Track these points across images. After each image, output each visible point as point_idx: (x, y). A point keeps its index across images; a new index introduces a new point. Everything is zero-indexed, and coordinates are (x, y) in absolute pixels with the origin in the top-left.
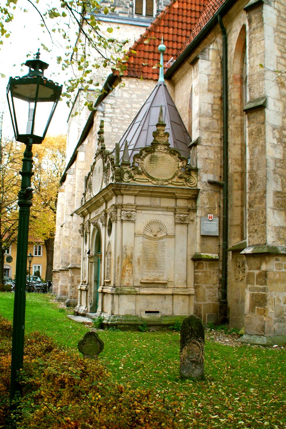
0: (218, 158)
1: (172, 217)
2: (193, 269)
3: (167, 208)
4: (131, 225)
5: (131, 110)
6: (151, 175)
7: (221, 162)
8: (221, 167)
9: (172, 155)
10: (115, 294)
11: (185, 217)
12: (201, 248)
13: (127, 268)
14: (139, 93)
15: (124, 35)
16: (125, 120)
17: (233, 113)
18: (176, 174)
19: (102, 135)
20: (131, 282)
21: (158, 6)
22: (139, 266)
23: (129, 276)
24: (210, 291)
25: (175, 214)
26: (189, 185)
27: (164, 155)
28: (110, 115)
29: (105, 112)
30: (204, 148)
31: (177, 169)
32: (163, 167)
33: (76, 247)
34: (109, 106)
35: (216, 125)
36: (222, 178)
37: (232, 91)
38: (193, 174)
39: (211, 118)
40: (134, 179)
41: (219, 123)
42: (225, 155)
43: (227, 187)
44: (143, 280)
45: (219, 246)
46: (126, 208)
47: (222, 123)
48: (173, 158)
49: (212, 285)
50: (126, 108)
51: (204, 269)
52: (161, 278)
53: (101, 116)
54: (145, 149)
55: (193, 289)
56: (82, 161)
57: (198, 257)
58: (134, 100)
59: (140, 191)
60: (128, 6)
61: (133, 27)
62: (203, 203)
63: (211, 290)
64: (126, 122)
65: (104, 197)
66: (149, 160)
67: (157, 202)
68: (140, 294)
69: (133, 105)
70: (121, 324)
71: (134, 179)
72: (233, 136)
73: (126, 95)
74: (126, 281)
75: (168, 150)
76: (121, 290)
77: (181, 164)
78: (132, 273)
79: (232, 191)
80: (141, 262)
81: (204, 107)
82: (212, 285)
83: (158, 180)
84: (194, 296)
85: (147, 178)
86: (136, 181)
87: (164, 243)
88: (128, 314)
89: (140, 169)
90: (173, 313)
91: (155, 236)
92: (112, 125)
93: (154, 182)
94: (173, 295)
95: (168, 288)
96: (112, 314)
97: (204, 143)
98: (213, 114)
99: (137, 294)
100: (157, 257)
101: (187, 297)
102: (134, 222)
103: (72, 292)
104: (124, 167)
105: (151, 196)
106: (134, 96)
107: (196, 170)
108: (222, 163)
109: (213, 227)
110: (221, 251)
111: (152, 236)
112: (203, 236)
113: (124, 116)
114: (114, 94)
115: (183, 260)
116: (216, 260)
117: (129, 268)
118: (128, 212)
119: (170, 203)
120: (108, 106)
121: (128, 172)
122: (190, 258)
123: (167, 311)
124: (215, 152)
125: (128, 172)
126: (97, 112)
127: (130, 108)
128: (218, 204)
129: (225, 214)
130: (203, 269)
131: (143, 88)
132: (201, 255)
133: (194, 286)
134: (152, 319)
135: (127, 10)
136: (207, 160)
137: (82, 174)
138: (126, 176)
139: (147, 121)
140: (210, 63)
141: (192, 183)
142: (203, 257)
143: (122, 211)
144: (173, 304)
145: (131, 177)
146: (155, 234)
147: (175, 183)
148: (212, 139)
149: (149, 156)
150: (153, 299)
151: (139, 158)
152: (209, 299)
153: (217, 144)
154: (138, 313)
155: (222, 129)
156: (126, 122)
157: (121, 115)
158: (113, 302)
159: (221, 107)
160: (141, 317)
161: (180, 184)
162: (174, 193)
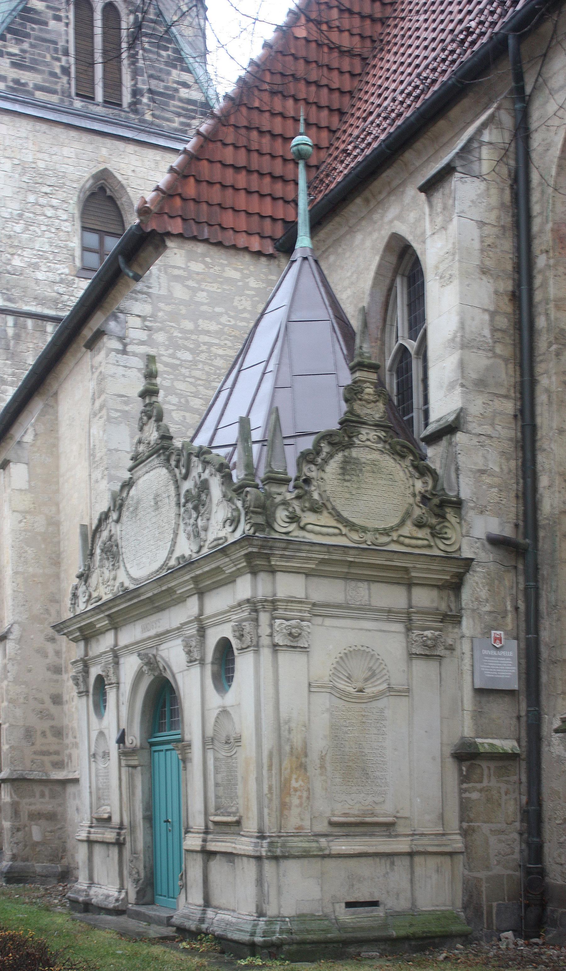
0: (510, 471)
1: (401, 638)
2: (456, 782)
3: (389, 611)
4: (299, 659)
5: (194, 337)
6: (345, 514)
7: (518, 484)
8: (517, 497)
9: (397, 458)
10: (268, 858)
11: (435, 639)
12: (476, 724)
13: (294, 784)
14: (214, 288)
16: (181, 365)
17: (556, 339)
18: (408, 514)
19: (154, 399)
20: (307, 824)
21: (134, 78)
22: (324, 778)
23: (301, 805)
24: (500, 841)
25: (409, 630)
26: (442, 547)
27: (375, 456)
28: (143, 349)
29: (127, 341)
30: (475, 440)
31: (411, 500)
32: (375, 493)
35: (504, 376)
36: (521, 529)
37: (550, 274)
38: (450, 515)
39: (490, 354)
40: (302, 524)
41: (511, 372)
42: (529, 464)
43: (536, 555)
44: (334, 815)
45: (519, 718)
46: (286, 610)
47: (517, 368)
48: (398, 467)
49: (504, 826)
50: (182, 331)
51: (485, 783)
52: (378, 809)
53: (117, 351)
54: (327, 436)
55: (458, 837)
56: (21, 490)
57: (472, 750)
58: (204, 308)
59: (323, 562)
60: (58, 71)
61: (73, 133)
62: (477, 599)
63: (503, 837)
64: (183, 370)
65: (196, 580)
66: (340, 471)
67: (362, 593)
68: (330, 856)
69: (200, 322)
70: (291, 943)
71: (302, 524)
72: (555, 406)
73: (179, 292)
74: (293, 821)
75: (385, 442)
76: (284, 845)
77: (419, 485)
78: (308, 798)
79: (553, 567)
81: (473, 319)
82: (504, 826)
83: (364, 530)
84: (461, 857)
85: (334, 524)
86: (309, 532)
87: (382, 711)
88: (305, 912)
89: (316, 496)
90: (414, 904)
91: (357, 689)
93: (355, 536)
94: (411, 854)
95: (397, 836)
96: (261, 914)
97: (473, 426)
98: (495, 342)
99: (324, 857)
100: (366, 751)
101: (448, 859)
102: (305, 650)
103: (17, 843)
104: (274, 489)
105: (346, 577)
106: (201, 296)
107: (458, 504)
108: (520, 488)
109: (504, 666)
110: (523, 734)
111: (352, 690)
112: (480, 692)
113: (179, 354)
114: (149, 287)
115: (434, 759)
116: (511, 757)
117: (300, 782)
118: (293, 622)
119: (392, 597)
120: (133, 321)
121: (285, 503)
122: (448, 751)
123: (397, 899)
124: (503, 453)
125: (285, 503)
126: (105, 338)
127: (191, 332)
128: (512, 601)
129: (532, 629)
130: (481, 782)
131: (225, 275)
133: (461, 828)
134: (366, 923)
135: (56, 83)
136: (484, 477)
137: (23, 524)
138: (281, 514)
139: (286, 360)
141: (447, 542)
142: (482, 750)
143: (274, 618)
144: (412, 881)
145: (294, 519)
146: (359, 685)
147: (407, 541)
148: (495, 413)
149: (339, 457)
150: (364, 868)
151: (312, 462)
152: (499, 862)
153: (506, 431)
154: (328, 910)
155: (518, 388)
156: (183, 370)
157: (170, 351)
158: (260, 882)
159: (515, 323)
160: (336, 919)
161: (420, 542)
162: (406, 570)
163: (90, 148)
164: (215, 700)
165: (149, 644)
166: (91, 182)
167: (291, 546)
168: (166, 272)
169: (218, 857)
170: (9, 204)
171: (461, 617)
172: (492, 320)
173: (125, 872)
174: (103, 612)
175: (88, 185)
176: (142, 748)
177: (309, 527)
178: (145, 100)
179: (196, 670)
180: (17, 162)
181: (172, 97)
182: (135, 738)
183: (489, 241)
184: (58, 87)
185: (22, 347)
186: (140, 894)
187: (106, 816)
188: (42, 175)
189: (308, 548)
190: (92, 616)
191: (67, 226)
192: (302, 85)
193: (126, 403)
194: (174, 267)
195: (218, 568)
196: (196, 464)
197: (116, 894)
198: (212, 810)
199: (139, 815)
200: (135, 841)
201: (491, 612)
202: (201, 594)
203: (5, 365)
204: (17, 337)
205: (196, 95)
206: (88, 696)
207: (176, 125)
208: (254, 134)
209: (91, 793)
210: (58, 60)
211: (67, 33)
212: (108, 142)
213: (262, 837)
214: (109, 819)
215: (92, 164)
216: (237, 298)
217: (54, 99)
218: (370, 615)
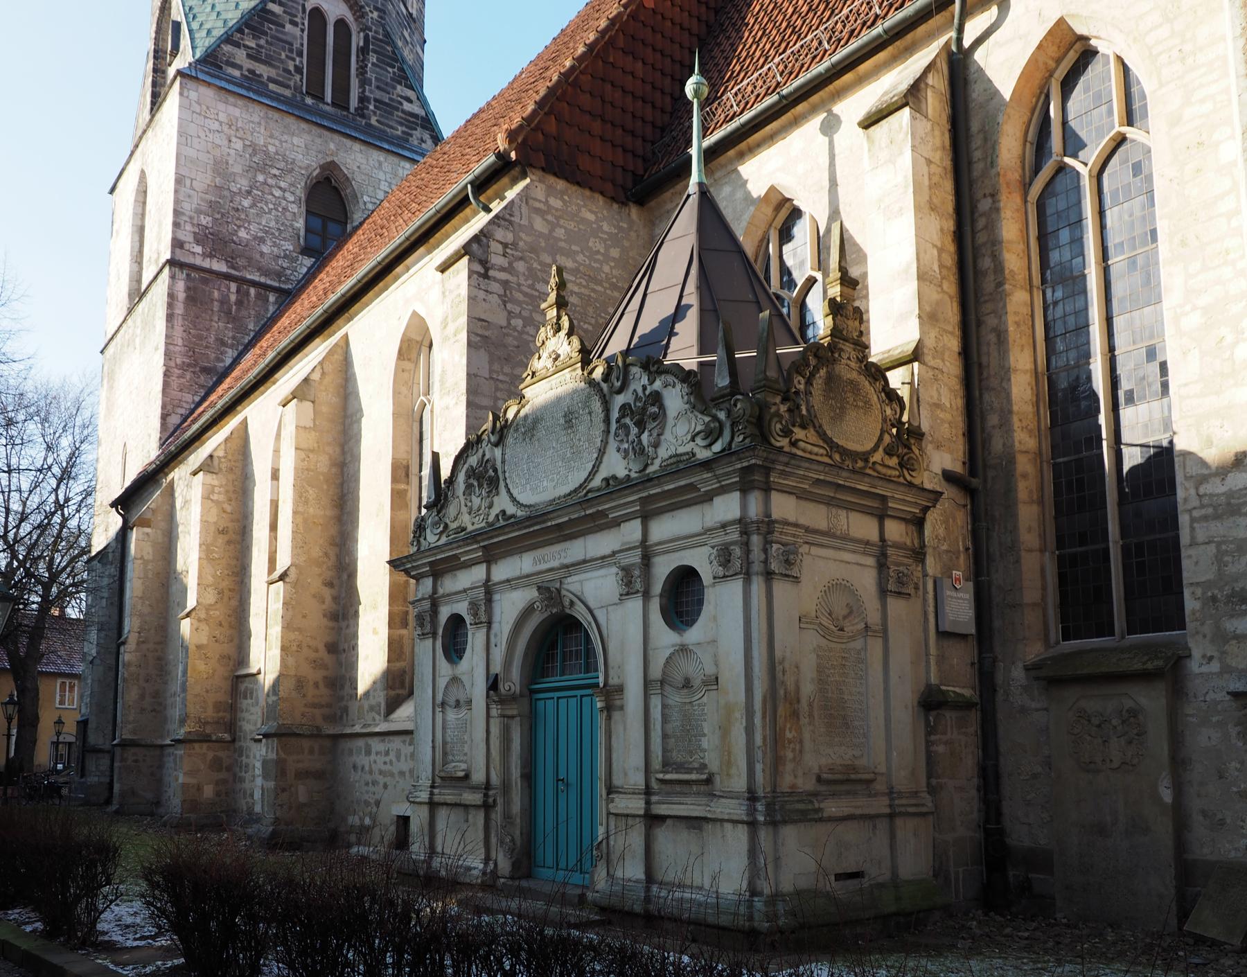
3: (508, 581)
10: (766, 823)
14: (572, 225)
15: (281, 142)
23: (794, 758)
28: (503, 276)
33: (292, 673)
34: (500, 248)
35: (950, 314)
50: (541, 263)
58: (562, 244)
60: (292, 68)
80: (816, 714)
92: (509, 306)
98: (943, 278)
102: (796, 580)
103: (281, 806)
106: (559, 233)
109: (960, 608)
114: (511, 215)
115: (906, 707)
130: (945, 733)
132: (943, 692)
133: (928, 784)
140: (929, 124)
157: (530, 282)
158: (753, 853)
162: (884, 499)
163: (318, 141)
164: (665, 638)
165: (549, 576)
166: (318, 171)
167: (793, 462)
168: (527, 203)
169: (669, 822)
170: (238, 179)
171: (924, 554)
172: (939, 256)
173: (493, 840)
174: (478, 542)
175: (315, 174)
176: (521, 695)
177: (801, 444)
178: (371, 107)
179: (635, 605)
180: (248, 143)
181: (397, 109)
182: (513, 682)
183: (936, 179)
184: (292, 84)
185: (244, 313)
186: (515, 865)
187: (461, 774)
188: (272, 159)
189: (807, 465)
190: (458, 547)
191: (294, 208)
192: (649, 50)
193: (486, 328)
194: (535, 199)
195: (691, 484)
196: (637, 376)
197: (481, 866)
198: (657, 763)
199: (516, 773)
200: (509, 804)
201: (947, 551)
202: (646, 517)
203: (226, 328)
204: (239, 303)
205: (415, 108)
206: (434, 638)
207: (399, 133)
208: (608, 87)
209: (434, 747)
210: (294, 60)
211: (302, 38)
212: (336, 137)
213: (752, 797)
214: (467, 777)
215: (320, 156)
216: (592, 240)
217: (288, 93)
218: (850, 546)
